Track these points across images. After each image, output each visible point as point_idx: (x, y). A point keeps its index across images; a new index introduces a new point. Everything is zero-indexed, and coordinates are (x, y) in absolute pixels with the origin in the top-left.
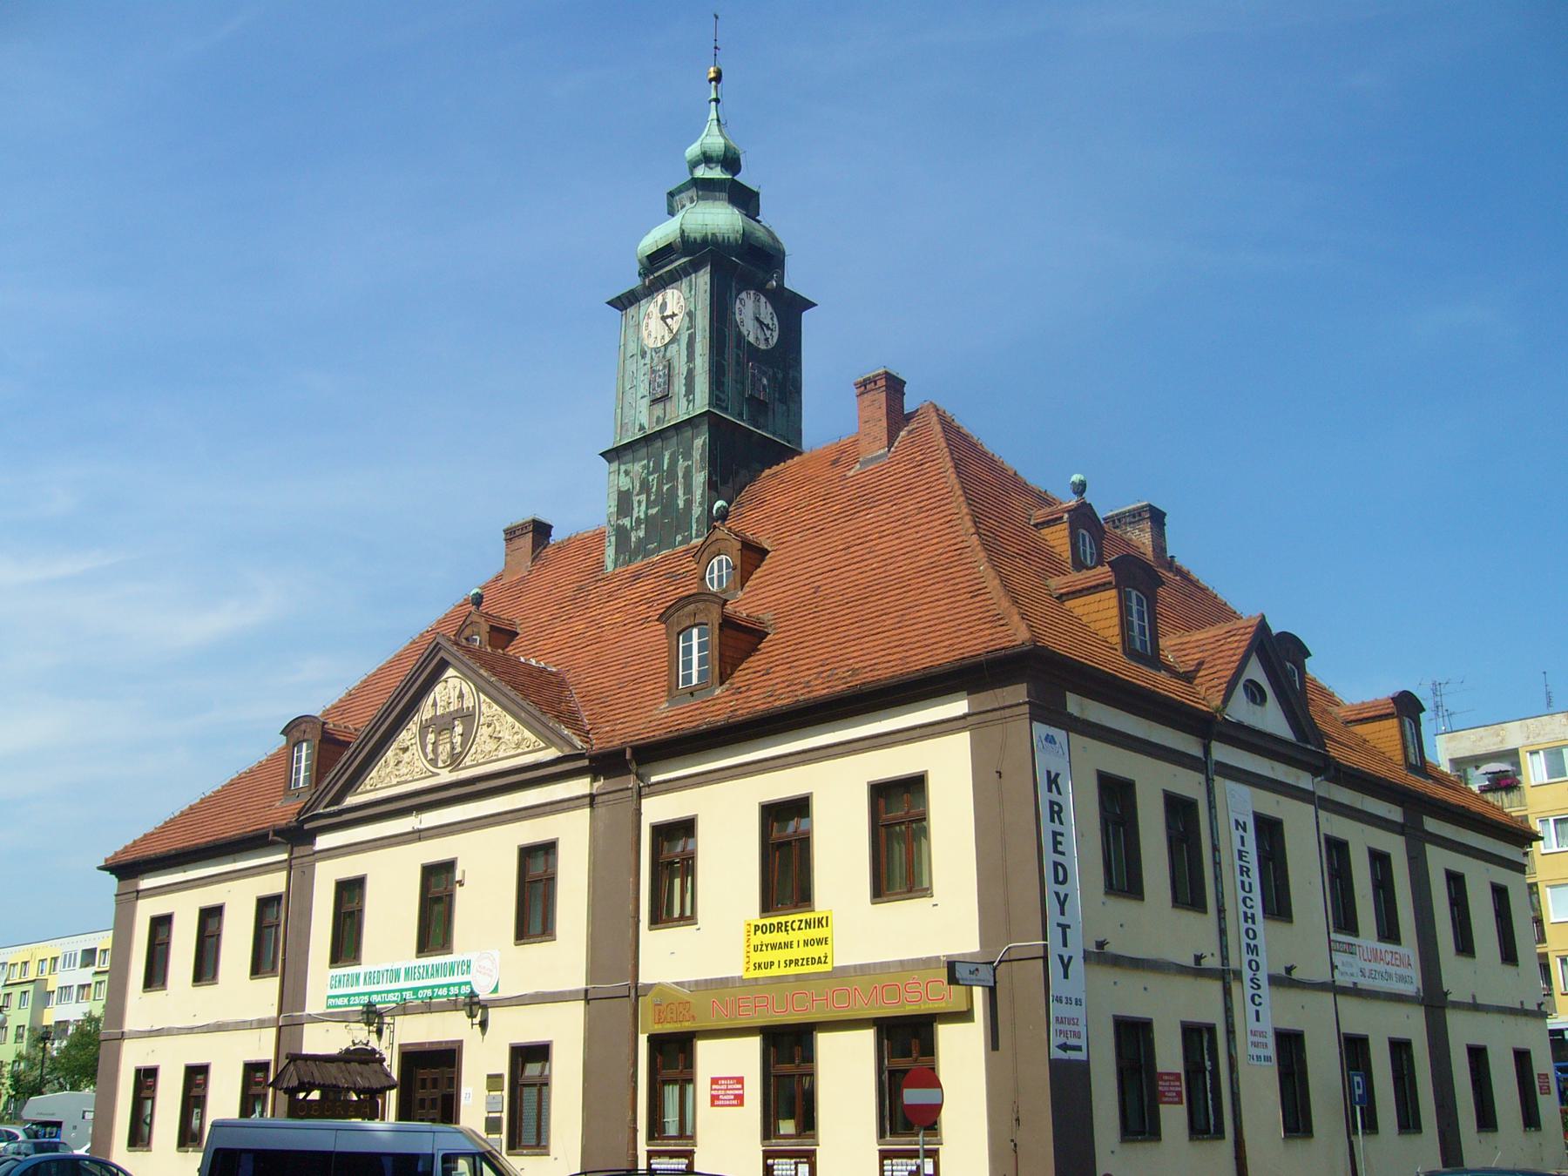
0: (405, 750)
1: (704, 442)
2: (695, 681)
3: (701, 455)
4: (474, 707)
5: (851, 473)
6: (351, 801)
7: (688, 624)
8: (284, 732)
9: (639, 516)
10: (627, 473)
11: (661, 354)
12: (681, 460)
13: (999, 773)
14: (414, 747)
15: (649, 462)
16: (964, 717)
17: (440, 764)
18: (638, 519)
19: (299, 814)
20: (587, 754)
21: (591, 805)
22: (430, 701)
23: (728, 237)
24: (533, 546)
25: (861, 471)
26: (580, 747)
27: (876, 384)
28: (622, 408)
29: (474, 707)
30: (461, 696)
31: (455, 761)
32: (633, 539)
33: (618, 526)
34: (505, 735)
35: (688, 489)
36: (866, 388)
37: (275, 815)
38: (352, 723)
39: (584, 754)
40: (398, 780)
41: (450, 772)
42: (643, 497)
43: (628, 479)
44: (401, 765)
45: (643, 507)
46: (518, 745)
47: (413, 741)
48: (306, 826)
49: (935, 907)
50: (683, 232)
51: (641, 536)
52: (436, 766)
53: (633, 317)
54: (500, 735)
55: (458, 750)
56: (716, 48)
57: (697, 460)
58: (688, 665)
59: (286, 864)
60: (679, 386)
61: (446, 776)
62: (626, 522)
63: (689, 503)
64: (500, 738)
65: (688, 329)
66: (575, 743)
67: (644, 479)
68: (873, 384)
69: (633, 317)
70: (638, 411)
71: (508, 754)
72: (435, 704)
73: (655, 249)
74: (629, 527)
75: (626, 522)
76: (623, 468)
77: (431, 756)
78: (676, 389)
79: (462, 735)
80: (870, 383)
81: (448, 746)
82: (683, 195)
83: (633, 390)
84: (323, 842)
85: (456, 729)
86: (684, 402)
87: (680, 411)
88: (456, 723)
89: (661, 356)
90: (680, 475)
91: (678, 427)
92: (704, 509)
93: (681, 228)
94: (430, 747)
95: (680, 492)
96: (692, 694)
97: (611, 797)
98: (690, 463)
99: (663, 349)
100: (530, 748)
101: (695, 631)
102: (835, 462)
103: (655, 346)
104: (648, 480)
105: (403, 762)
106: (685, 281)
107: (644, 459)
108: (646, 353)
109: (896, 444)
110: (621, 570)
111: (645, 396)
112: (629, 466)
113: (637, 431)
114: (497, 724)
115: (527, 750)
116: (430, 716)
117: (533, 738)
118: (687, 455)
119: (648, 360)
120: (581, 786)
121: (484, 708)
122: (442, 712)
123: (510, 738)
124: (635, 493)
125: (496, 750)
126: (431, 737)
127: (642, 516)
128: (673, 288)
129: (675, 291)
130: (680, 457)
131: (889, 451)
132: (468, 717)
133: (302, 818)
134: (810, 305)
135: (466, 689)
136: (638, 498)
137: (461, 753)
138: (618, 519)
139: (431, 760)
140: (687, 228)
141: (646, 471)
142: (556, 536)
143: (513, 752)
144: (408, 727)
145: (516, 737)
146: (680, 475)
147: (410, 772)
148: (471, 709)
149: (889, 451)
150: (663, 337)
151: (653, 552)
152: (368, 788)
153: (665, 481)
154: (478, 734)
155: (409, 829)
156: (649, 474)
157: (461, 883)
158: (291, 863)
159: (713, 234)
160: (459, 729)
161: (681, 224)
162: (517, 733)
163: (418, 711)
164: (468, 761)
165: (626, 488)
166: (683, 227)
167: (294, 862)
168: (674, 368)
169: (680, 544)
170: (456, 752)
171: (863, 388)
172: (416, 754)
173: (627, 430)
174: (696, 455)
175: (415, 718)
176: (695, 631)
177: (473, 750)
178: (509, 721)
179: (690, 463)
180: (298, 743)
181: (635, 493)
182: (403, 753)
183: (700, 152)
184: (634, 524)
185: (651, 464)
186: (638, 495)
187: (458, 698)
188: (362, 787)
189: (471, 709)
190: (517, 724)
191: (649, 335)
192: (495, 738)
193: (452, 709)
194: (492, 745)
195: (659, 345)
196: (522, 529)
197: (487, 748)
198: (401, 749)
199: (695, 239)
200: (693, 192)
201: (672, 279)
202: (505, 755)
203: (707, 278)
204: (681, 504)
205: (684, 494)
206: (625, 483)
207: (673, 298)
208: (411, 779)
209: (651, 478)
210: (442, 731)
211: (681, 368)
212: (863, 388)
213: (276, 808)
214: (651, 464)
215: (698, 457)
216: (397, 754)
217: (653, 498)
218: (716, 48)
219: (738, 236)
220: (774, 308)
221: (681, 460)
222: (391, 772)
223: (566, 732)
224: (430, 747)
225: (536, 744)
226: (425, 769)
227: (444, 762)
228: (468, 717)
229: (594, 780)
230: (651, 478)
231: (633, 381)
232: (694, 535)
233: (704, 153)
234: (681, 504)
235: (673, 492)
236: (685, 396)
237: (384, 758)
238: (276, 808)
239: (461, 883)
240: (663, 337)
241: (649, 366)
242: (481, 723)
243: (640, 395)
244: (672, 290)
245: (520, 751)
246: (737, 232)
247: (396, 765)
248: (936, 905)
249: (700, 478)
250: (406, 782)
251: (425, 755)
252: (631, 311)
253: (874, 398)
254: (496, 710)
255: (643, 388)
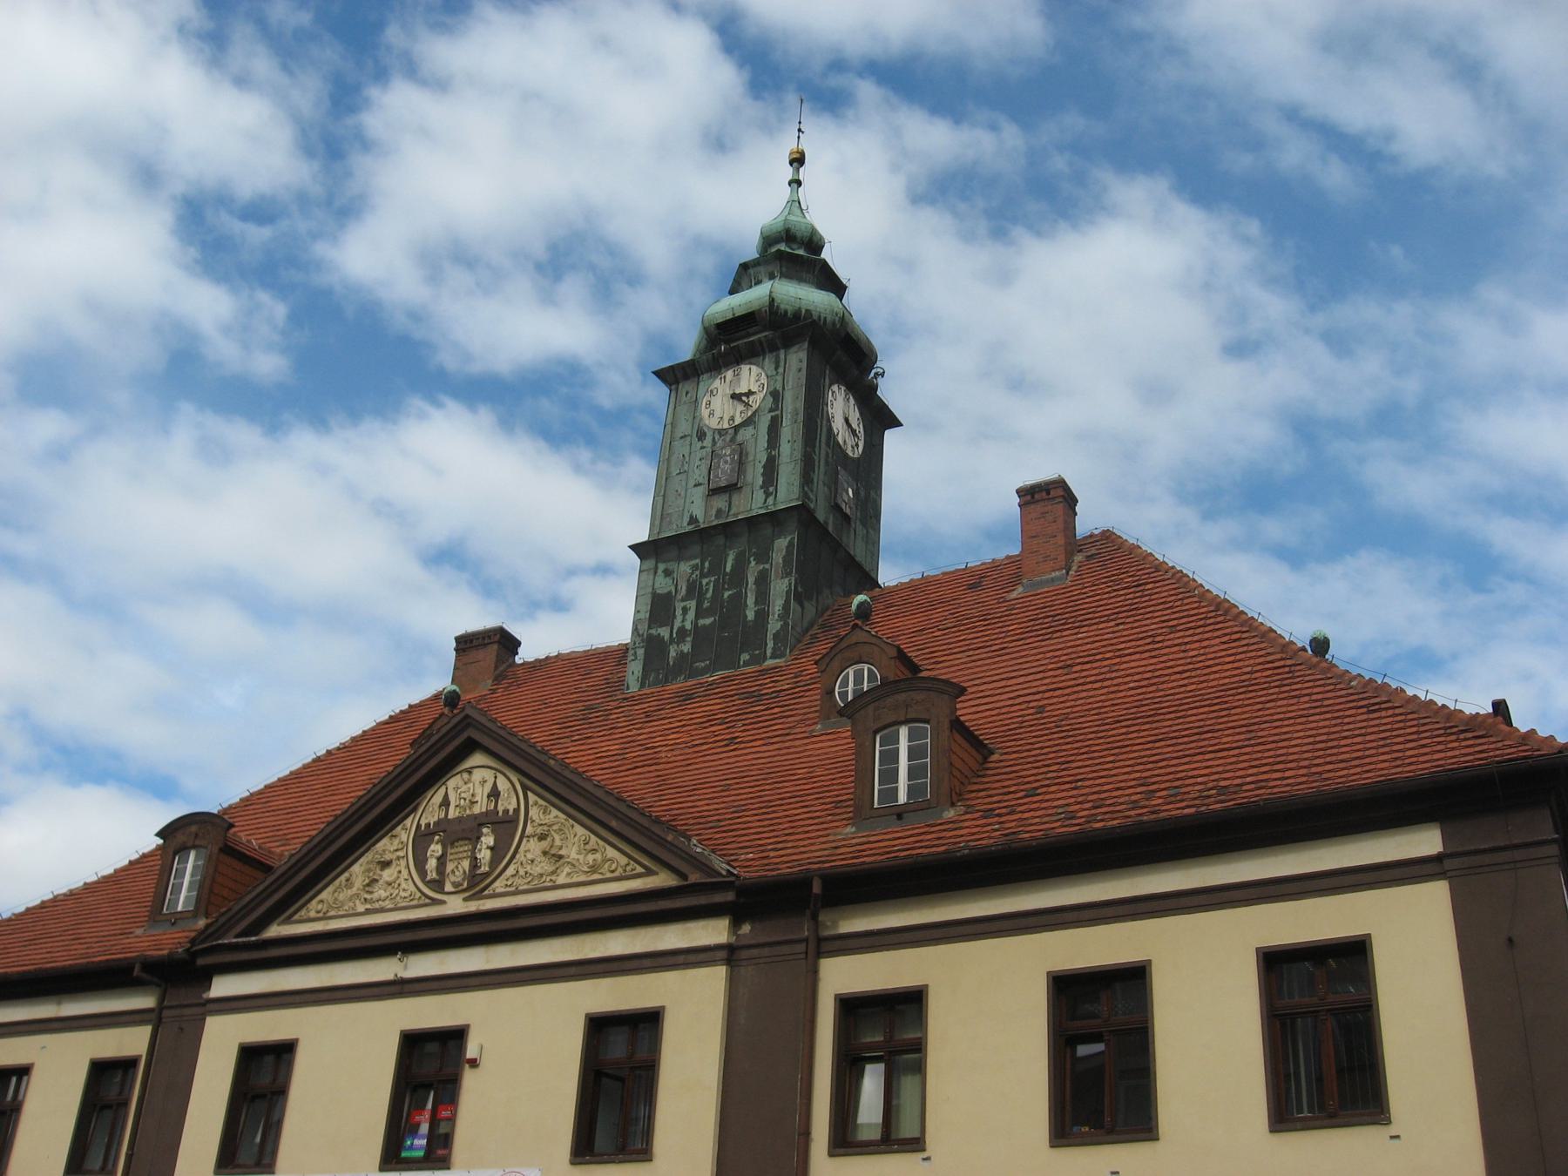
0: (386, 864)
1: (791, 544)
2: (902, 798)
3: (784, 558)
4: (517, 811)
5: (1014, 595)
6: (275, 931)
7: (892, 718)
8: (160, 834)
9: (683, 627)
10: (667, 573)
11: (728, 438)
12: (753, 563)
13: (1510, 940)
14: (403, 862)
15: (702, 564)
16: (1437, 859)
17: (448, 887)
18: (682, 631)
19: (193, 941)
20: (737, 883)
21: (729, 962)
22: (438, 798)
23: (825, 318)
24: (497, 661)
25: (1022, 595)
26: (724, 873)
27: (1048, 493)
28: (664, 496)
29: (517, 811)
30: (495, 794)
31: (476, 883)
32: (673, 654)
33: (650, 636)
34: (572, 853)
35: (763, 596)
36: (1033, 497)
37: (137, 945)
38: (255, 837)
39: (732, 882)
40: (368, 906)
41: (465, 900)
42: (692, 604)
43: (669, 580)
44: (376, 887)
45: (691, 615)
46: (594, 868)
47: (401, 854)
48: (201, 961)
49: (1396, 1141)
50: (772, 300)
51: (686, 651)
52: (442, 891)
53: (687, 393)
54: (561, 852)
55: (485, 869)
56: (799, 130)
57: (777, 563)
58: (890, 776)
59: (153, 1016)
60: (755, 475)
61: (455, 905)
62: (664, 632)
63: (762, 616)
64: (561, 857)
65: (771, 411)
66: (717, 867)
67: (694, 581)
68: (1044, 494)
69: (687, 393)
70: (688, 500)
71: (575, 879)
72: (446, 803)
73: (731, 317)
74: (667, 637)
75: (664, 632)
76: (662, 567)
77: (431, 875)
78: (749, 478)
79: (492, 849)
80: (1041, 491)
81: (466, 864)
82: (761, 269)
83: (683, 477)
84: (223, 986)
85: (483, 839)
86: (759, 495)
87: (752, 503)
88: (485, 830)
89: (728, 439)
90: (751, 580)
91: (752, 522)
92: (786, 624)
93: (770, 296)
94: (432, 864)
95: (751, 601)
96: (900, 817)
97: (766, 951)
98: (767, 566)
99: (731, 431)
100: (617, 874)
101: (903, 732)
102: (971, 587)
103: (720, 427)
104: (701, 583)
105: (381, 882)
106: (768, 361)
107: (696, 558)
108: (705, 434)
109: (1074, 568)
110: (648, 692)
111: (700, 484)
112: (672, 566)
113: (685, 524)
114: (557, 837)
115: (609, 875)
116: (436, 819)
117: (623, 860)
118: (764, 556)
119: (708, 442)
120: (713, 932)
121: (533, 812)
122: (457, 814)
123: (581, 857)
124: (679, 597)
125: (553, 873)
126: (436, 849)
127: (688, 626)
128: (751, 363)
129: (754, 368)
130: (752, 559)
131: (1067, 573)
132: (505, 825)
133: (194, 949)
134: (897, 424)
135: (503, 784)
136: (683, 604)
137: (487, 875)
138: (649, 628)
139: (433, 881)
140: (778, 297)
141: (698, 572)
142: (525, 654)
143: (583, 878)
144: (394, 832)
145: (590, 858)
146: (751, 580)
147: (391, 897)
148: (511, 812)
149: (1067, 573)
150: (732, 419)
151: (703, 672)
152: (313, 914)
153: (726, 586)
154: (522, 849)
155: (390, 977)
156: (703, 576)
157: (474, 1063)
158: (160, 1013)
159: (807, 310)
160: (488, 840)
161: (771, 292)
162: (594, 851)
163: (415, 810)
164: (499, 886)
165: (666, 591)
166: (774, 295)
167: (166, 1013)
168: (747, 454)
169: (746, 664)
170: (478, 872)
171: (1029, 497)
172: (405, 873)
173: (670, 523)
174: (778, 557)
175: (408, 822)
176: (903, 732)
177: (511, 871)
178: (579, 834)
179: (767, 566)
180: (183, 850)
181: (679, 597)
182: (382, 870)
183: (782, 228)
184: (675, 635)
185: (707, 564)
186: (683, 600)
187: (489, 796)
188: (303, 912)
189: (511, 812)
190: (593, 838)
191: (712, 414)
192: (553, 855)
193: (477, 810)
194: (544, 866)
195: (726, 426)
196: (484, 638)
197: (537, 870)
198: (379, 862)
199: (786, 312)
200: (775, 268)
201: (737, 358)
202: (568, 881)
203: (803, 355)
204: (750, 615)
205: (756, 603)
206: (663, 585)
207: (751, 378)
208: (393, 906)
209: (704, 581)
210: (457, 841)
211: (759, 454)
212: (1029, 497)
213: (136, 937)
214: (707, 564)
215: (781, 561)
216: (369, 870)
217: (706, 604)
218: (799, 130)
219: (837, 319)
220: (861, 414)
221: (753, 563)
222: (358, 895)
223: (699, 850)
224: (432, 864)
225: (628, 868)
226: (418, 895)
227: (455, 884)
228: (505, 825)
229: (736, 924)
230: (704, 581)
231: (683, 465)
232: (768, 654)
233: (788, 231)
234: (750, 615)
235: (738, 601)
236: (761, 488)
237: (346, 875)
238: (136, 937)
239: (474, 1063)
240: (732, 419)
241: (709, 450)
242: (527, 833)
243: (691, 483)
244: (748, 366)
245: (596, 876)
246: (837, 314)
247: (368, 885)
248: (1397, 1137)
249: (780, 587)
250: (382, 910)
251: (422, 872)
252: (685, 387)
253: (1046, 509)
254: (557, 817)
255: (699, 474)
